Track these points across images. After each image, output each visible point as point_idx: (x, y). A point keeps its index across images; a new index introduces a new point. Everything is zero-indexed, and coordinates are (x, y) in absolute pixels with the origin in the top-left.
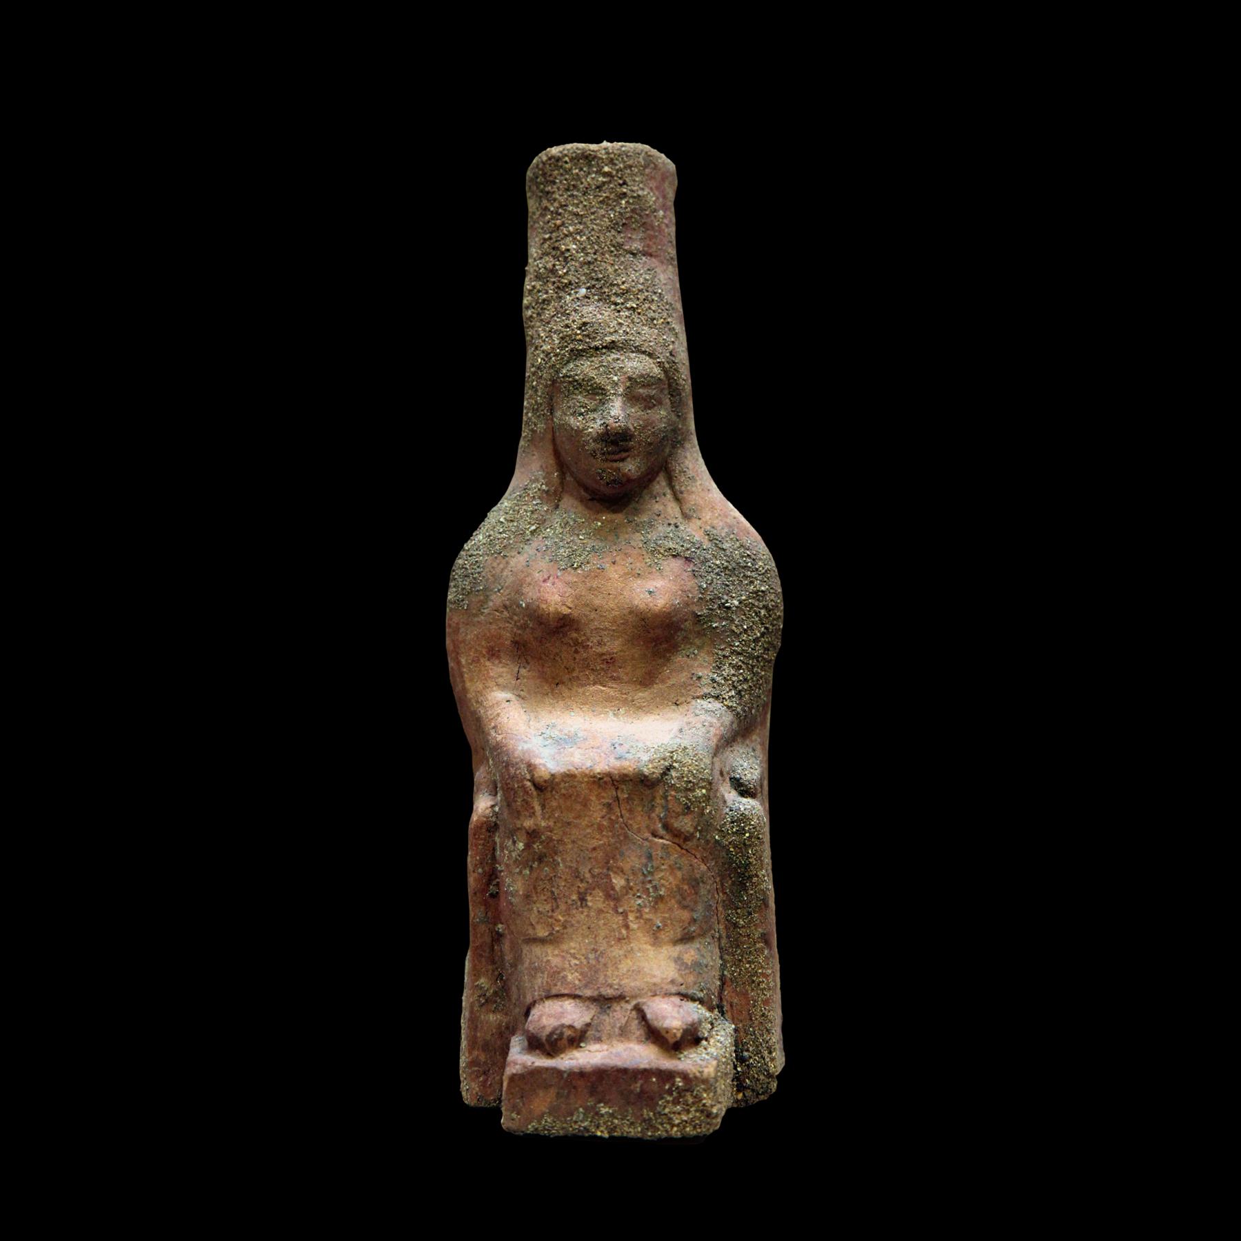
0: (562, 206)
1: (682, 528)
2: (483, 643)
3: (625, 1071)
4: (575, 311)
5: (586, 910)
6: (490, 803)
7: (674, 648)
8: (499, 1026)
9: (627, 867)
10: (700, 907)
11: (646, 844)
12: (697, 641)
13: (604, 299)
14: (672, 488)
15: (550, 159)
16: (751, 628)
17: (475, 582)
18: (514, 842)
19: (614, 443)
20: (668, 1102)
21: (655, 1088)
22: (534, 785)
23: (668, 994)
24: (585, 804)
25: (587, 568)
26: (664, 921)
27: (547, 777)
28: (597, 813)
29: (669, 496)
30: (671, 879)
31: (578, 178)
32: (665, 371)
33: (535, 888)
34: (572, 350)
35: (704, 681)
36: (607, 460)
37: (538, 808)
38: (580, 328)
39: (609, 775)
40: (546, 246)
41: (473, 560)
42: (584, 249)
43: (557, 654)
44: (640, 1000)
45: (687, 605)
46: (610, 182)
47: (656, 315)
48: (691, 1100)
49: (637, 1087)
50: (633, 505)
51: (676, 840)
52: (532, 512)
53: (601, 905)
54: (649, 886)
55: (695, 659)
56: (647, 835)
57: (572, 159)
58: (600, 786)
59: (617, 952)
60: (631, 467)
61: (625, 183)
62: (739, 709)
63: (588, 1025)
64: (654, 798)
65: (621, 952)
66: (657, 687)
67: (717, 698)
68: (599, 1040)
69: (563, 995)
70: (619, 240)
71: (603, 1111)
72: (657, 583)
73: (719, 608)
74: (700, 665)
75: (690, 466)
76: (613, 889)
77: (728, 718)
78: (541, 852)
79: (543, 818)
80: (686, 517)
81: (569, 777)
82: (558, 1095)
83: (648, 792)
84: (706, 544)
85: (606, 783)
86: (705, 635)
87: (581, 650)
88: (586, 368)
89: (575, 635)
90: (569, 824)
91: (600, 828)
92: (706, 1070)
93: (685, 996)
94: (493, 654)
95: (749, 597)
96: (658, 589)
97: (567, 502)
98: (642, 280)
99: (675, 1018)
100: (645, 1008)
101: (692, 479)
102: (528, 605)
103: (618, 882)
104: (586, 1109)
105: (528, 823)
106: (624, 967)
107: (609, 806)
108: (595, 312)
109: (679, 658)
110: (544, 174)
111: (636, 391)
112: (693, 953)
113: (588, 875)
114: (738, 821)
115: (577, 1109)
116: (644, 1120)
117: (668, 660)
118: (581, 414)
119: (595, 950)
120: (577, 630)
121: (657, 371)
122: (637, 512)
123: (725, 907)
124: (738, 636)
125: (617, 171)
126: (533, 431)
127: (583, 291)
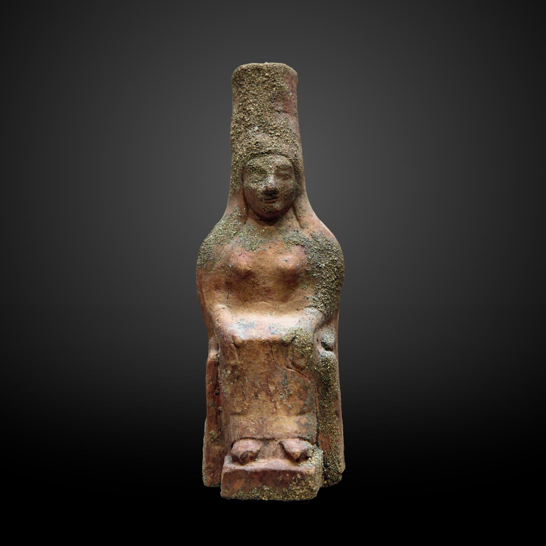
0: (247, 91)
1: (300, 232)
2: (213, 283)
3: (275, 471)
4: (253, 137)
5: (258, 400)
6: (215, 353)
7: (296, 285)
8: (220, 451)
9: (276, 382)
10: (308, 399)
11: (284, 371)
12: (307, 282)
13: (266, 131)
14: (296, 215)
15: (242, 70)
16: (330, 276)
17: (209, 256)
18: (226, 371)
19: (270, 195)
20: (294, 485)
21: (288, 479)
22: (235, 345)
23: (294, 438)
24: (258, 354)
25: (258, 250)
26: (292, 405)
27: (241, 342)
28: (263, 358)
29: (294, 218)
30: (295, 387)
31: (254, 78)
32: (293, 163)
33: (235, 391)
34: (252, 154)
35: (310, 300)
36: (267, 202)
37: (237, 355)
38: (255, 144)
39: (268, 341)
40: (240, 108)
41: (208, 246)
42: (257, 110)
43: (245, 288)
44: (281, 440)
45: (302, 266)
46: (268, 80)
47: (289, 139)
48: (304, 484)
49: (280, 478)
50: (279, 222)
51: (298, 370)
52: (234, 225)
53: (264, 398)
54: (285, 390)
55: (306, 290)
56: (285, 367)
57: (252, 70)
58: (264, 346)
59: (271, 419)
60: (278, 205)
61: (275, 81)
62: (325, 312)
63: (259, 451)
64: (288, 351)
65: (273, 419)
66: (289, 302)
67: (315, 307)
68: (263, 457)
69: (248, 438)
70: (272, 105)
71: (265, 489)
72: (289, 257)
73: (316, 267)
74: (308, 293)
75: (304, 205)
76: (270, 391)
77: (320, 316)
78: (238, 375)
79: (239, 360)
80: (302, 227)
81: (250, 342)
82: (246, 482)
83: (285, 348)
84: (311, 240)
85: (266, 344)
86: (310, 279)
87: (256, 286)
88: (258, 162)
89: (253, 279)
90: (250, 362)
91: (264, 364)
92: (311, 471)
93: (301, 438)
94: (217, 288)
95: (330, 263)
96: (290, 259)
97: (250, 221)
98: (282, 123)
99: (297, 448)
100: (284, 443)
102: (232, 266)
103: (272, 388)
104: (258, 488)
105: (232, 362)
106: (275, 425)
107: (268, 354)
108: (262, 137)
109: (299, 290)
110: (239, 77)
111: (280, 172)
112: (305, 419)
113: (259, 385)
114: (325, 361)
115: (254, 488)
116: (284, 493)
117: (294, 290)
118: (256, 182)
119: (262, 418)
120: (254, 277)
121: (289, 163)
122: (280, 225)
123: (319, 399)
124: (325, 280)
125: (272, 75)
126: (234, 189)
127: (256, 128)
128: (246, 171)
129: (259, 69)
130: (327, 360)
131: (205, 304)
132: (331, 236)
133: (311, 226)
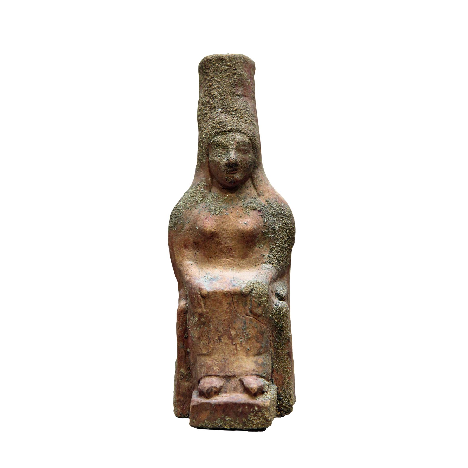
0: (212, 78)
1: (257, 199)
2: (182, 242)
3: (236, 404)
4: (217, 117)
5: (221, 343)
6: (185, 303)
7: (254, 244)
8: (188, 387)
9: (236, 327)
10: (264, 342)
11: (244, 318)
12: (263, 242)
13: (228, 113)
14: (253, 184)
15: (207, 60)
16: (283, 237)
17: (179, 220)
18: (194, 318)
19: (232, 167)
20: (252, 416)
21: (247, 410)
22: (202, 296)
23: (252, 375)
24: (221, 303)
25: (221, 214)
26: (250, 347)
27: (206, 293)
28: (225, 307)
29: (252, 187)
30: (253, 331)
31: (218, 67)
32: (251, 140)
33: (202, 335)
34: (216, 132)
35: (265, 257)
36: (229, 173)
37: (203, 305)
38: (219, 124)
39: (230, 292)
40: (206, 93)
41: (178, 211)
42: (220, 94)
43: (210, 247)
44: (241, 377)
45: (259, 228)
46: (230, 69)
47: (248, 119)
48: (260, 415)
49: (240, 410)
50: (239, 190)
51: (255, 317)
52: (201, 193)
53: (226, 341)
54: (245, 334)
55: (262, 249)
56: (244, 315)
57: (216, 60)
58: (226, 296)
59: (233, 359)
60: (238, 176)
61: (236, 69)
62: (279, 267)
63: (222, 387)
64: (247, 301)
65: (234, 359)
66: (248, 259)
67: (270, 263)
68: (226, 392)
69: (212, 375)
70: (233, 90)
71: (228, 419)
72: (248, 220)
73: (271, 229)
75: (260, 176)
76: (231, 335)
77: (275, 271)
79: (205, 309)
80: (259, 195)
81: (215, 293)
82: (211, 413)
83: (244, 299)
84: (266, 205)
85: (228, 295)
86: (266, 239)
87: (219, 245)
88: (221, 139)
89: (217, 239)
90: (215, 311)
91: (226, 312)
92: (266, 404)
93: (258, 376)
94: (186, 246)
95: (282, 225)
97: (214, 189)
98: (242, 106)
99: (254, 384)
100: (243, 380)
102: (199, 228)
103: (233, 333)
104: (221, 418)
105: (199, 311)
106: (235, 365)
107: (230, 304)
108: (224, 118)
109: (256, 248)
110: (205, 66)
112: (261, 359)
113: (222, 330)
114: (278, 310)
115: (218, 418)
116: (243, 423)
117: (252, 249)
118: (219, 156)
119: (224, 358)
120: (218, 238)
121: (248, 140)
122: (240, 193)
123: (274, 342)
124: (278, 240)
125: (233, 64)
126: (201, 162)
127: (220, 110)
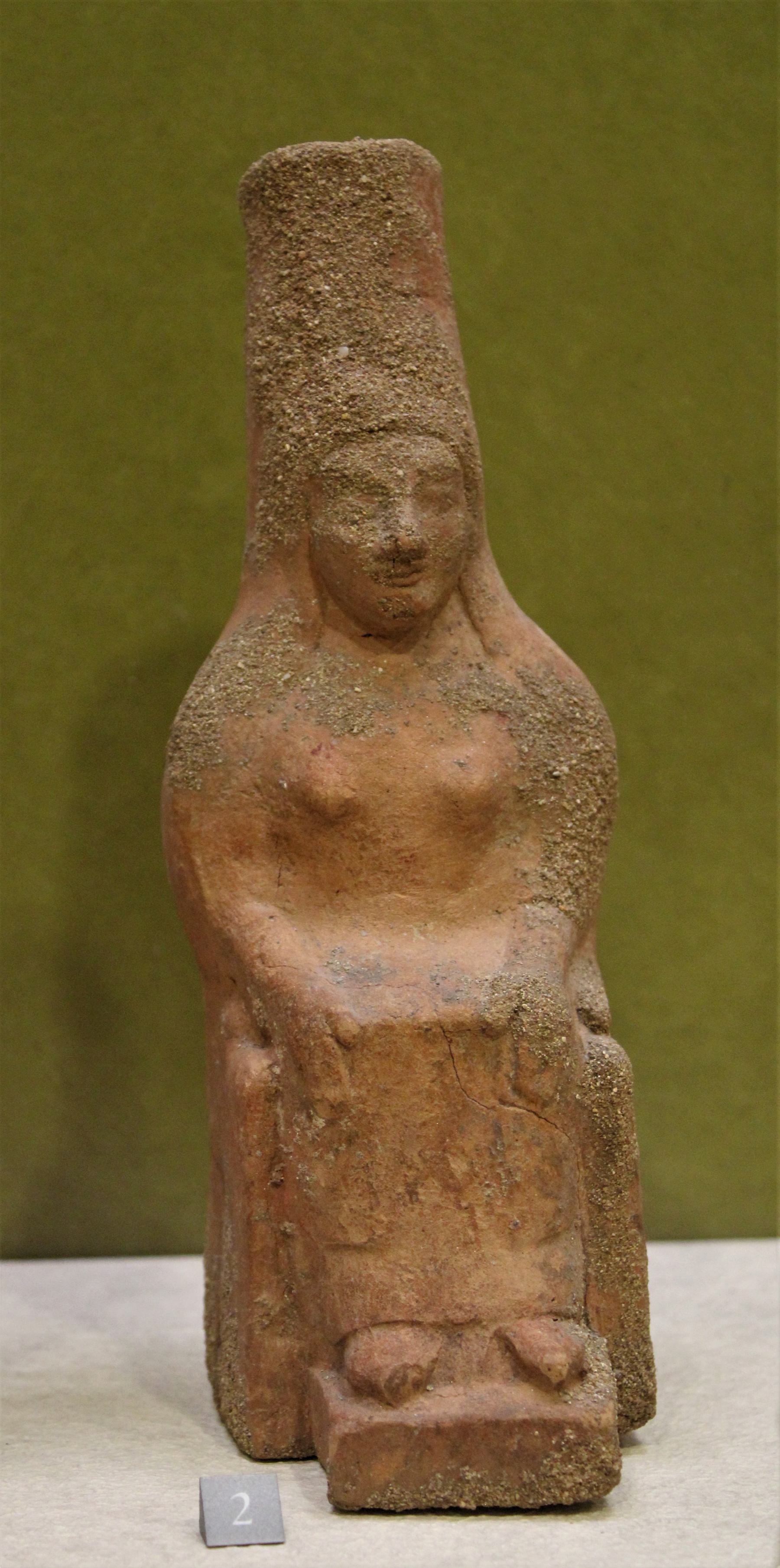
0: (304, 231)
1: (487, 669)
2: (227, 836)
3: (497, 1424)
4: (337, 378)
5: (417, 1207)
6: (266, 1062)
7: (491, 836)
8: (289, 1354)
9: (469, 1147)
10: (565, 1193)
11: (492, 1113)
12: (519, 825)
13: (374, 359)
14: (469, 613)
15: (283, 165)
16: (585, 802)
17: (211, 753)
18: (310, 1117)
19: (407, 562)
20: (555, 1460)
21: (538, 1442)
22: (338, 1041)
23: (537, 1314)
24: (409, 1064)
25: (372, 733)
26: (521, 1216)
27: (356, 1030)
28: (424, 1076)
29: (466, 626)
30: (529, 1161)
31: (326, 191)
32: (460, 457)
33: (344, 1178)
34: (337, 434)
35: (532, 878)
36: (394, 585)
37: (344, 1071)
38: (346, 403)
39: (440, 1024)
40: (285, 286)
41: (205, 721)
42: (341, 291)
43: (334, 852)
44: (501, 1325)
45: (507, 777)
46: (370, 197)
47: (444, 381)
48: (585, 1456)
49: (513, 1444)
50: (423, 641)
51: (532, 1107)
52: (283, 654)
53: (437, 1199)
54: (499, 1170)
55: (518, 849)
56: (493, 1101)
57: (316, 165)
58: (427, 1041)
59: (463, 1260)
60: (424, 592)
61: (389, 198)
62: (578, 914)
63: (435, 1361)
64: (499, 1053)
65: (470, 1261)
66: (473, 891)
67: (550, 900)
68: (451, 1379)
69: (396, 1322)
70: (388, 278)
71: (469, 1476)
72: (468, 751)
73: (546, 777)
74: (521, 855)
75: (489, 582)
76: (452, 1176)
77: (567, 928)
78: (349, 1132)
79: (353, 1085)
80: (490, 653)
81: (385, 1028)
82: (407, 1460)
83: (491, 1044)
84: (521, 692)
85: (435, 1035)
86: (529, 816)
87: (370, 846)
88: (357, 458)
89: (359, 826)
90: (387, 1091)
91: (430, 1096)
92: (604, 1417)
93: (558, 1315)
94: (242, 850)
95: (581, 761)
96: (469, 759)
97: (332, 638)
98: (420, 332)
99: (555, 1349)
100: (509, 1334)
101: (493, 600)
102: (291, 786)
103: (459, 1166)
104: (446, 1473)
105: (333, 1094)
106: (477, 1279)
107: (439, 1065)
108: (365, 381)
109: (498, 849)
110: (275, 186)
111: (432, 490)
112: (560, 1254)
113: (417, 1160)
114: (603, 1072)
115: (434, 1474)
116: (524, 1485)
117: (484, 853)
118: (354, 522)
119: (434, 1260)
120: (363, 819)
121: (451, 460)
122: (428, 651)
123: (588, 1185)
124: (570, 813)
125: (379, 180)
126: (276, 541)
127: (344, 351)
128: (321, 485)
129: (338, 163)
130: (605, 1071)
131: (202, 899)
132: (576, 676)
133: (515, 643)
